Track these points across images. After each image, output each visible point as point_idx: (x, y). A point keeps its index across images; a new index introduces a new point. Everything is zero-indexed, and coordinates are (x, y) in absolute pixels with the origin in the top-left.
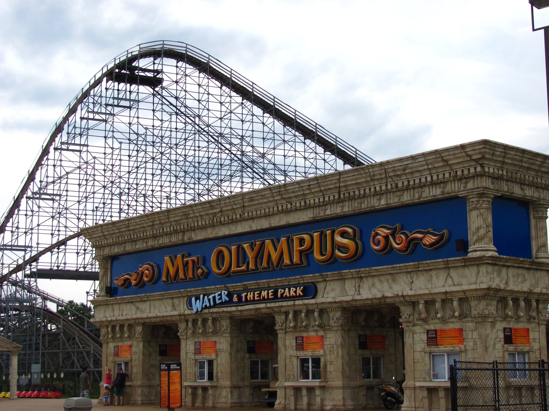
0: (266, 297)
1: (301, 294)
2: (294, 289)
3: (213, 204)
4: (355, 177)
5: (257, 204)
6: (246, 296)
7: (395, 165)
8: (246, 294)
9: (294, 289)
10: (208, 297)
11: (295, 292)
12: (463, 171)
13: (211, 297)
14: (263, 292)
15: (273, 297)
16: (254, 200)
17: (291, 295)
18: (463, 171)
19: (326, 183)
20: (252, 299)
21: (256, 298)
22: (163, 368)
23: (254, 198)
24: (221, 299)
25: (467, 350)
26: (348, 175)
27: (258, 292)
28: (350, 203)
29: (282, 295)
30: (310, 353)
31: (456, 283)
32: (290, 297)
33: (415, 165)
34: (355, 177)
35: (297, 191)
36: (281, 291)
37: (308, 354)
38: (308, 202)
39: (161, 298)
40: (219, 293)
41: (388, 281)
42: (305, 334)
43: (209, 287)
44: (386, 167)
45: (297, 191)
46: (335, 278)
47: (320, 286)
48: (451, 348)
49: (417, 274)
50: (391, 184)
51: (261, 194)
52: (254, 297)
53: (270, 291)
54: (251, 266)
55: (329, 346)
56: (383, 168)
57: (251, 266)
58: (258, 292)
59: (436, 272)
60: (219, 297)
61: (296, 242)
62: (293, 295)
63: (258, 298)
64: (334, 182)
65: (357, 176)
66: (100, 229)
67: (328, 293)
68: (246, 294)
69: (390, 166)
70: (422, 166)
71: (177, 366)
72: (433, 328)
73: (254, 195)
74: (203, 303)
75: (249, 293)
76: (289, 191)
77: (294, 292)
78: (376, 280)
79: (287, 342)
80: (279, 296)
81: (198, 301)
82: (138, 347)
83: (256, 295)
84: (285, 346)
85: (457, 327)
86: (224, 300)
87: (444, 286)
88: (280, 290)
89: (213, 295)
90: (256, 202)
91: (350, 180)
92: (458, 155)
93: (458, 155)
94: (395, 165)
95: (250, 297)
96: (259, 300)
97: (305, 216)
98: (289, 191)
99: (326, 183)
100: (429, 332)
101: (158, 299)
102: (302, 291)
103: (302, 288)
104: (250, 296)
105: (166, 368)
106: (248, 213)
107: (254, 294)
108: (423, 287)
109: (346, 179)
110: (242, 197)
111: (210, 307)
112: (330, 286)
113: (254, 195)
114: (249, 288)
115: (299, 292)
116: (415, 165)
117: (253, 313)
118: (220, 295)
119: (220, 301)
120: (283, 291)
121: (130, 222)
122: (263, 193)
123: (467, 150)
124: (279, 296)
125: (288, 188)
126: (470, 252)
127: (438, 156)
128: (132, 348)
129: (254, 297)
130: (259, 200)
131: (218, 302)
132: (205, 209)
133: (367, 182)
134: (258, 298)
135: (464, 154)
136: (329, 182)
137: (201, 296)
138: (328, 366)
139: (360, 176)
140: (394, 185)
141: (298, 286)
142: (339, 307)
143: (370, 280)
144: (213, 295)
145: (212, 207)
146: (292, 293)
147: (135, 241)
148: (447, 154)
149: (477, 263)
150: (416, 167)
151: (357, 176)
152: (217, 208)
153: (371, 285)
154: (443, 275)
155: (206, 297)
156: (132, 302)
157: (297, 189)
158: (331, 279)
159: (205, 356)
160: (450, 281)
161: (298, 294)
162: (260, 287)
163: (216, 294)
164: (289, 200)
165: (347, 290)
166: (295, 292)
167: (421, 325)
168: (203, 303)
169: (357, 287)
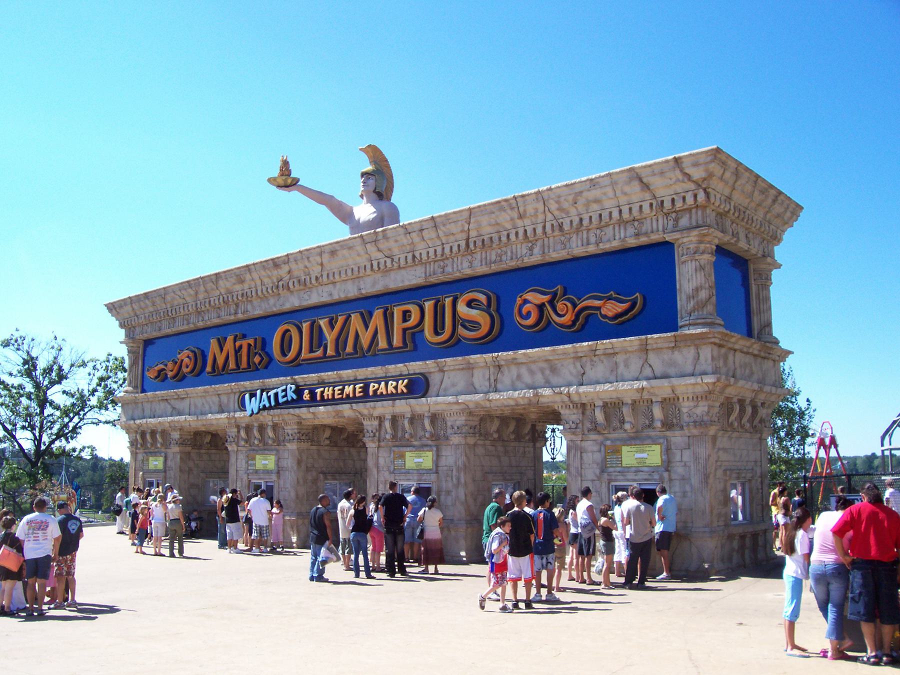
0: (351, 395)
1: (405, 391)
9: (394, 383)
11: (396, 388)
13: (272, 393)
15: (361, 394)
20: (330, 397)
24: (286, 396)
27: (341, 387)
32: (387, 395)
52: (333, 395)
53: (357, 386)
54: (330, 352)
57: (330, 352)
58: (341, 387)
63: (340, 396)
68: (322, 389)
77: (394, 387)
80: (371, 393)
83: (337, 392)
86: (290, 399)
88: (372, 384)
95: (328, 395)
96: (342, 399)
103: (406, 381)
107: (334, 391)
118: (285, 390)
119: (285, 399)
120: (376, 386)
124: (371, 393)
129: (333, 395)
131: (281, 400)
134: (340, 396)
146: (391, 388)
153: (515, 377)
155: (264, 394)
161: (399, 391)
169: (492, 380)
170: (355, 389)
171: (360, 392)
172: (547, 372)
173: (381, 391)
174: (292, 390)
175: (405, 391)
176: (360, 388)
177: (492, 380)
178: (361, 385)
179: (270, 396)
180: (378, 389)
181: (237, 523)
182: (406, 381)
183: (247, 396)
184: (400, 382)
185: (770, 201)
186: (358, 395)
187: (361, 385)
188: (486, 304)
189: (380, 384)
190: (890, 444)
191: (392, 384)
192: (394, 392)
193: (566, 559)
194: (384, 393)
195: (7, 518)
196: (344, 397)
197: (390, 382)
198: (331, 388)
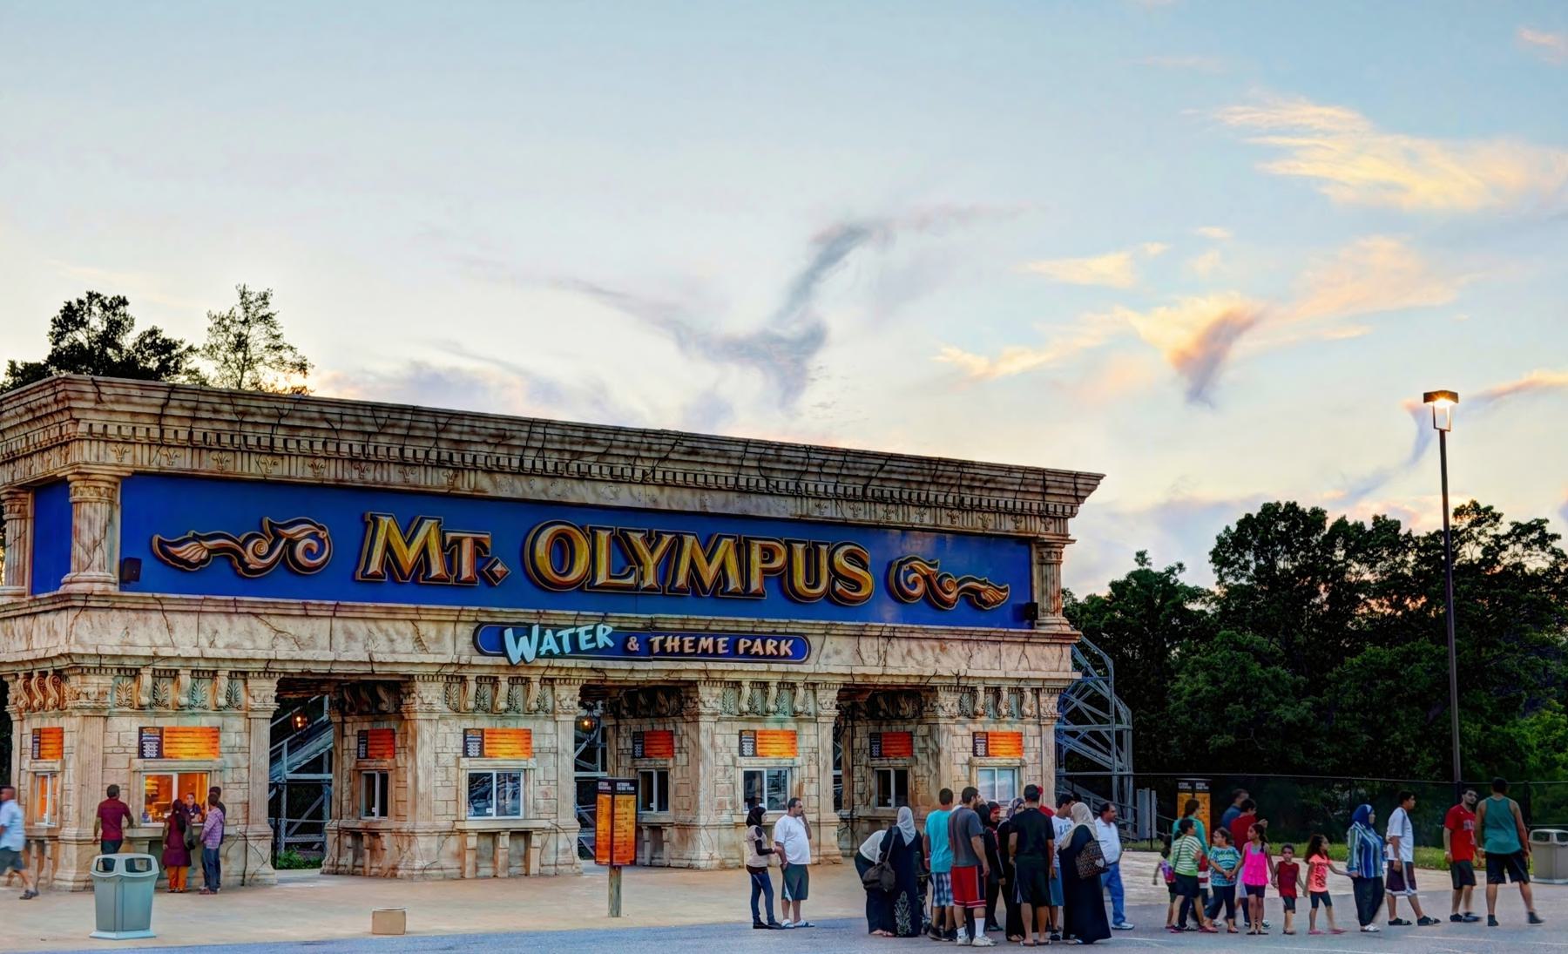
0: (711, 651)
1: (790, 653)
2: (775, 643)
3: (594, 435)
4: (911, 470)
5: (702, 463)
6: (662, 643)
7: (979, 471)
8: (662, 638)
9: (775, 643)
10: (554, 633)
11: (777, 648)
12: (787, 483)
13: (565, 634)
14: (703, 639)
15: (727, 651)
16: (697, 454)
17: (768, 653)
18: (787, 483)
19: (858, 465)
20: (677, 650)
21: (687, 650)
22: (624, 789)
23: (701, 451)
24: (594, 640)
25: (398, 767)
26: (902, 464)
27: (693, 638)
28: (799, 503)
29: (747, 650)
30: (773, 761)
31: (1033, 667)
32: (765, 656)
33: (1006, 480)
34: (911, 470)
35: (796, 463)
36: (745, 643)
37: (765, 764)
38: (803, 486)
39: (1048, 641)
40: (591, 627)
41: (933, 649)
42: (757, 727)
43: (664, 616)
44: (965, 470)
45: (796, 463)
46: (847, 633)
47: (815, 642)
48: (1010, 761)
49: (231, 622)
50: (954, 497)
51: (722, 447)
52: (681, 646)
53: (720, 640)
54: (650, 580)
55: (807, 750)
56: (960, 469)
57: (650, 580)
58: (693, 638)
59: (1007, 646)
60: (590, 636)
61: (756, 556)
62: (606, 644)
63: (693, 650)
64: (872, 467)
65: (915, 470)
66: (527, 429)
67: (827, 657)
68: (662, 638)
69: (972, 471)
70: (1013, 484)
71: (631, 785)
72: (982, 730)
73: (706, 445)
74: (540, 644)
75: (670, 638)
76: (782, 458)
78: (914, 645)
79: (719, 740)
80: (741, 651)
81: (524, 640)
82: (818, 738)
83: (687, 645)
84: (713, 745)
85: (1014, 730)
86: (601, 645)
87: (1017, 669)
88: (742, 641)
89: (572, 631)
90: (700, 459)
91: (900, 473)
92: (1065, 485)
93: (1065, 485)
94: (979, 471)
95: (673, 647)
96: (695, 654)
97: (785, 508)
98: (782, 458)
99: (858, 465)
100: (145, 731)
101: (1043, 643)
102: (791, 648)
103: (791, 642)
104: (672, 643)
105: (609, 788)
106: (664, 473)
108: (988, 667)
109: (894, 468)
110: (674, 441)
111: (562, 655)
112: (831, 644)
113: (706, 445)
114: (658, 625)
115: (785, 648)
116: (1006, 480)
117: (663, 676)
118: (593, 632)
119: (592, 645)
121: (453, 421)
122: (726, 447)
123: (1080, 481)
124: (741, 651)
125: (784, 453)
126: (65, 583)
127: (1041, 477)
128: (223, 737)
129: (681, 646)
130: (707, 456)
131: (583, 646)
132: (567, 439)
133: (920, 483)
134: (693, 650)
135: (1072, 485)
136: (863, 466)
137: (536, 630)
138: (805, 785)
139: (919, 471)
140: (957, 499)
141: (783, 638)
142: (438, 674)
143: (904, 643)
144: (572, 631)
145: (589, 441)
146: (770, 648)
147: (382, 463)
148: (1053, 478)
149: (1061, 641)
150: (1004, 483)
151: (915, 470)
152: (600, 445)
153: (905, 652)
154: (1016, 650)
155: (549, 632)
156: (256, 615)
157: (800, 460)
158: (841, 632)
159: (500, 763)
160: (1025, 664)
161: (783, 653)
162: (686, 627)
163: (581, 631)
164: (766, 473)
165: (864, 656)
166: (777, 648)
167: (964, 724)
168: (540, 644)
169: (881, 652)
170: (715, 645)
171: (724, 648)
172: (938, 651)
173: (549, 648)
174: (607, 633)
175: (790, 653)
176: (724, 642)
177: (881, 652)
178: (727, 639)
179: (561, 637)
180: (751, 647)
181: (866, 923)
182: (791, 642)
183: (509, 633)
184: (784, 642)
185: (558, 446)
186: (720, 651)
187: (727, 639)
188: (629, 533)
189: (753, 641)
190: (616, 910)
191: (604, 630)
192: (776, 653)
193: (1004, 909)
194: (762, 653)
195: (1114, 617)
196: (699, 651)
197: (769, 641)
198: (677, 638)
